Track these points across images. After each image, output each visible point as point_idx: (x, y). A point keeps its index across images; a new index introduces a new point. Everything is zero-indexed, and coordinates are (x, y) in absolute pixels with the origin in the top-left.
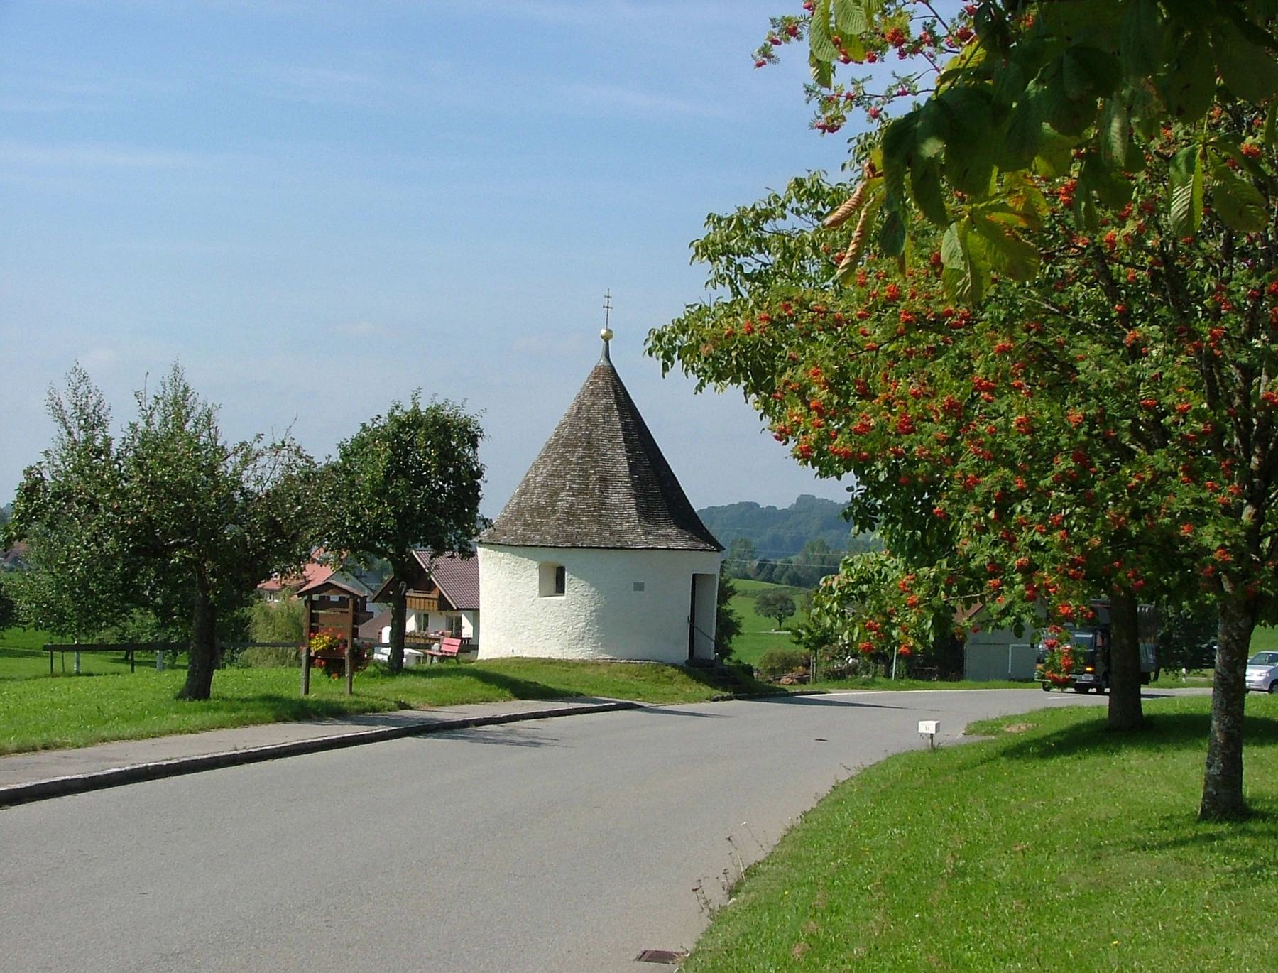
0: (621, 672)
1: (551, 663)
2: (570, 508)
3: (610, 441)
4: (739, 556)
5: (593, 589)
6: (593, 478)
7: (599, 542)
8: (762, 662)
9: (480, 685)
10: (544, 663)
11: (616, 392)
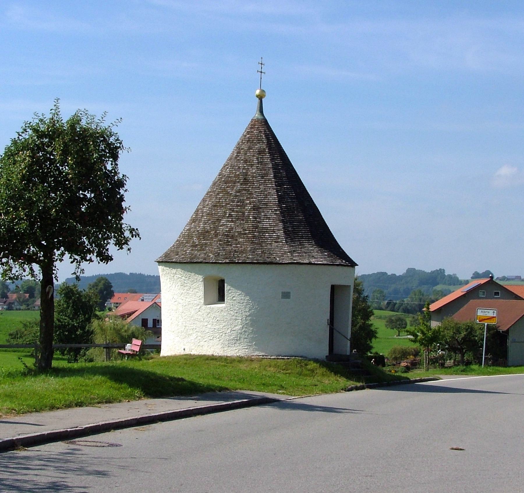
0: (270, 366)
1: (212, 359)
2: (229, 231)
3: (262, 177)
4: (377, 299)
5: (248, 298)
6: (249, 207)
7: (252, 259)
8: (389, 354)
9: (110, 383)
10: (207, 359)
11: (268, 139)
